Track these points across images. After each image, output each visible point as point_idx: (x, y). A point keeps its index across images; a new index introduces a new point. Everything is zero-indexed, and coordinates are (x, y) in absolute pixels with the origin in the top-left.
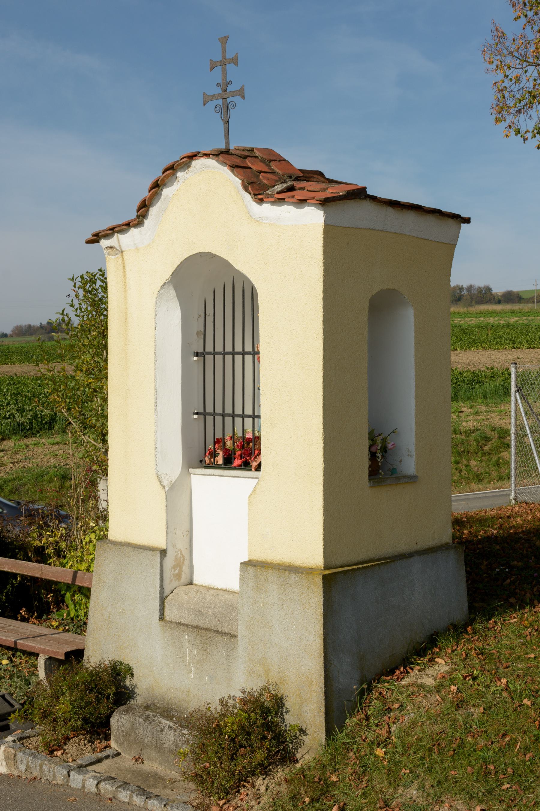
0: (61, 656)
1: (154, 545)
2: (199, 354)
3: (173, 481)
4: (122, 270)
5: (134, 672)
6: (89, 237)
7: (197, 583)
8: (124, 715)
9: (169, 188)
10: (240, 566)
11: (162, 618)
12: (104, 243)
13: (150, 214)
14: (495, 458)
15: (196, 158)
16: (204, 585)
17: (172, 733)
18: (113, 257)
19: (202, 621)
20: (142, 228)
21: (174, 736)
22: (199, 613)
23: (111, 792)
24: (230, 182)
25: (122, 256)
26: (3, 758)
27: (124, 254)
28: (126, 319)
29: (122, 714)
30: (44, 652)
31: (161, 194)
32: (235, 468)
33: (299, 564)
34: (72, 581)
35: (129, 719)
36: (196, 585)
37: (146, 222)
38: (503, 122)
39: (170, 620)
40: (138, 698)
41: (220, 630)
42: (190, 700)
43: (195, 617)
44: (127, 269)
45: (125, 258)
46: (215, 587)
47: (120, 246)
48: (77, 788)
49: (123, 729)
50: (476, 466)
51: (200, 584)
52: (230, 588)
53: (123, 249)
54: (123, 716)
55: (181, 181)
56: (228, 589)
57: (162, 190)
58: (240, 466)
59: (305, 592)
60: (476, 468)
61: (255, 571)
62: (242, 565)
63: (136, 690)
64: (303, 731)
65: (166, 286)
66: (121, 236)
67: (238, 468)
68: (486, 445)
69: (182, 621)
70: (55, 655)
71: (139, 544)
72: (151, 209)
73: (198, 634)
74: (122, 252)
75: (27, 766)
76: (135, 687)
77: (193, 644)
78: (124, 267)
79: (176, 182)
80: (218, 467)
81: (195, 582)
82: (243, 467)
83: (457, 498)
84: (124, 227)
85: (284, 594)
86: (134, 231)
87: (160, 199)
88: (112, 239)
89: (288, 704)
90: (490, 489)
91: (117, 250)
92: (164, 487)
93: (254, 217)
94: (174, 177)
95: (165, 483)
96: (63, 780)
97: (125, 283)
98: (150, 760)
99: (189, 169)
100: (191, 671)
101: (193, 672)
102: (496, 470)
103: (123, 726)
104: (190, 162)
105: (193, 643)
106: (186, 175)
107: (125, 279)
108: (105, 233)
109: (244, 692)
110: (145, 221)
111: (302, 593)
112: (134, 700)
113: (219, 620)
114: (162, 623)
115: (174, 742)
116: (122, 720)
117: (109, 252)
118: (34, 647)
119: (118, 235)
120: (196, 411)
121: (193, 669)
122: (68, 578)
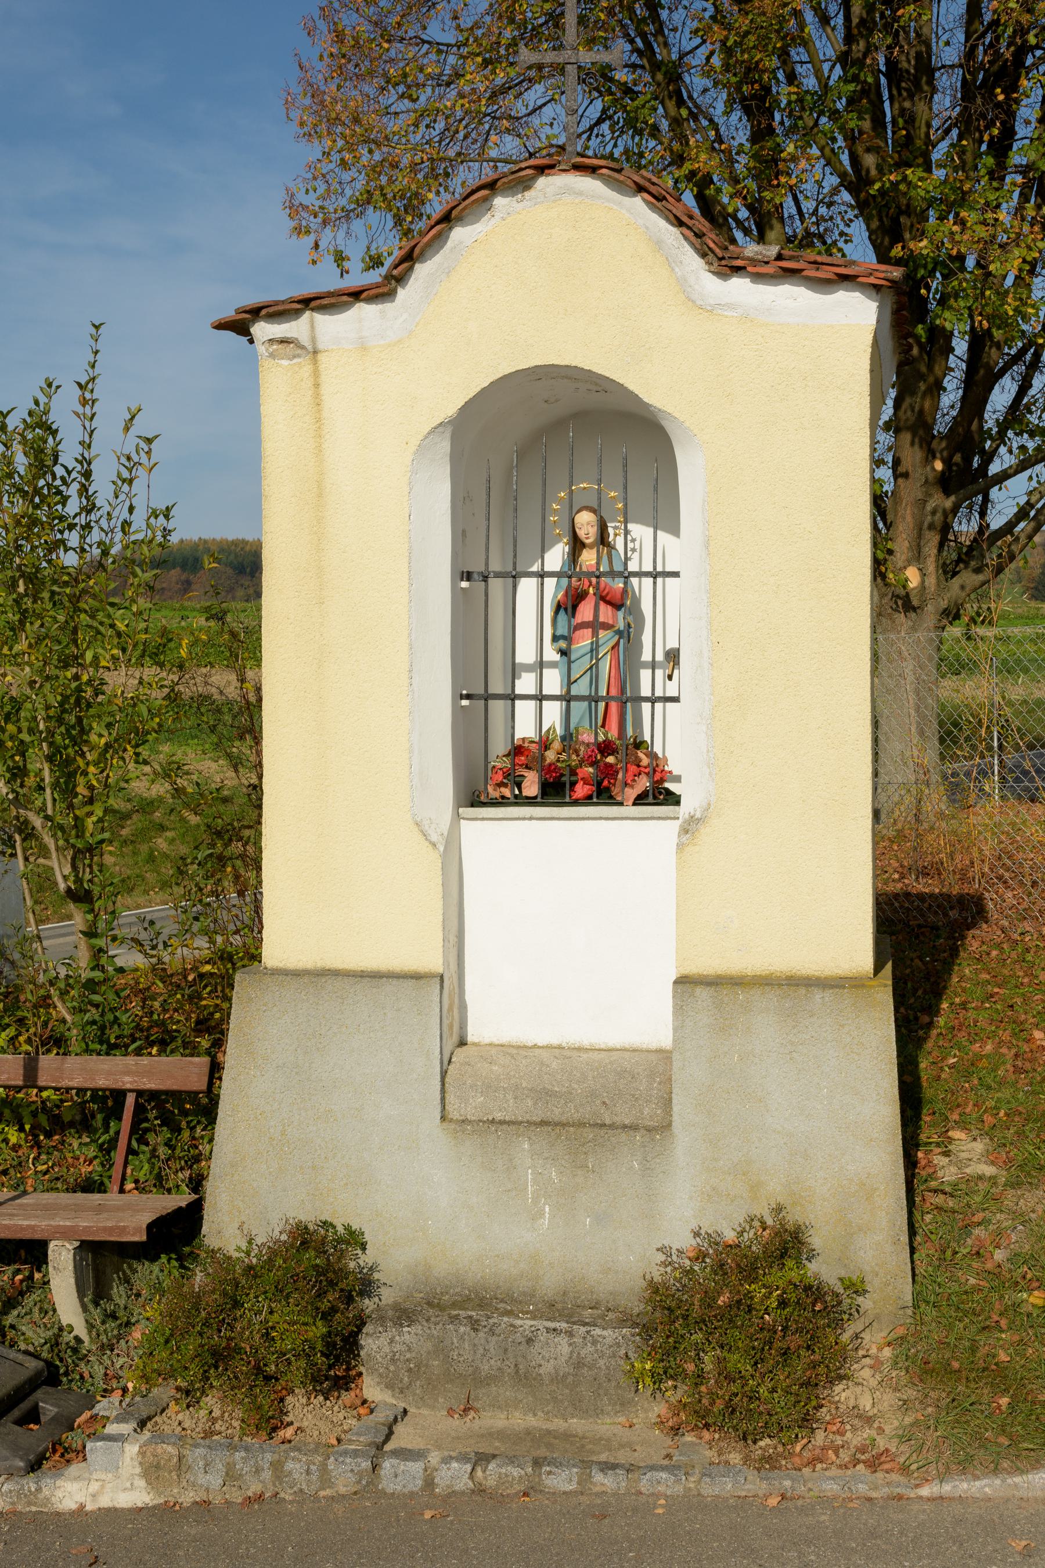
0: (132, 1235)
1: (406, 969)
2: (475, 576)
3: (446, 834)
4: (310, 393)
5: (367, 1237)
6: (228, 313)
7: (477, 1041)
8: (408, 1326)
9: (469, 228)
10: (675, 992)
11: (443, 1118)
12: (262, 330)
13: (413, 276)
14: (144, 848)
15: (552, 171)
16: (497, 1042)
17: (563, 1341)
18: (285, 363)
19: (557, 1111)
20: (389, 305)
21: (570, 1345)
22: (545, 1095)
23: (519, 1481)
24: (636, 229)
25: (315, 362)
26: (138, 1470)
27: (321, 357)
28: (320, 495)
29: (401, 1325)
30: (65, 1234)
31: (448, 237)
32: (575, 803)
33: (813, 973)
34: (24, 1080)
35: (428, 1331)
36: (474, 1044)
37: (401, 293)
38: (293, 224)
39: (463, 1118)
40: (384, 1292)
41: (608, 1122)
42: (541, 1273)
43: (535, 1104)
44: (326, 390)
45: (322, 367)
46: (530, 1044)
47: (313, 340)
48: (406, 1491)
49: (408, 1356)
50: (115, 865)
51: (487, 1041)
52: (572, 1041)
53: (321, 346)
54: (406, 1329)
55: (498, 215)
56: (564, 1045)
57: (451, 229)
58: (590, 797)
59: (850, 1021)
60: (117, 868)
61: (716, 994)
62: (680, 986)
63: (376, 1276)
64: (857, 1288)
65: (441, 429)
66: (320, 318)
67: (587, 801)
68: (123, 827)
69: (499, 1116)
70: (110, 1235)
71: (360, 969)
72: (417, 266)
73: (559, 1136)
74: (315, 352)
75: (227, 1474)
76: (371, 1269)
77: (546, 1158)
78: (317, 386)
79: (488, 215)
80: (531, 801)
81: (470, 1038)
82: (595, 800)
83: (51, 933)
84: (345, 298)
85: (795, 1031)
86: (363, 310)
87: (442, 247)
88: (293, 323)
89: (816, 1240)
90: (157, 904)
91: (303, 347)
92: (434, 845)
93: (699, 303)
94: (486, 205)
95: (434, 838)
96: (359, 1482)
97: (318, 420)
98: (499, 1407)
99: (526, 193)
100: (541, 1214)
101: (547, 1215)
102: (153, 871)
103: (409, 1350)
104: (533, 179)
105: (546, 1155)
106: (515, 204)
107: (319, 411)
108: (280, 308)
109: (697, 1234)
110: (400, 291)
111: (843, 1026)
112: (369, 1297)
113: (604, 1103)
114: (445, 1125)
115: (570, 1358)
116: (407, 1336)
117: (274, 350)
118: (32, 1227)
119: (315, 314)
120: (464, 692)
121: (547, 1209)
122: (9, 1073)
